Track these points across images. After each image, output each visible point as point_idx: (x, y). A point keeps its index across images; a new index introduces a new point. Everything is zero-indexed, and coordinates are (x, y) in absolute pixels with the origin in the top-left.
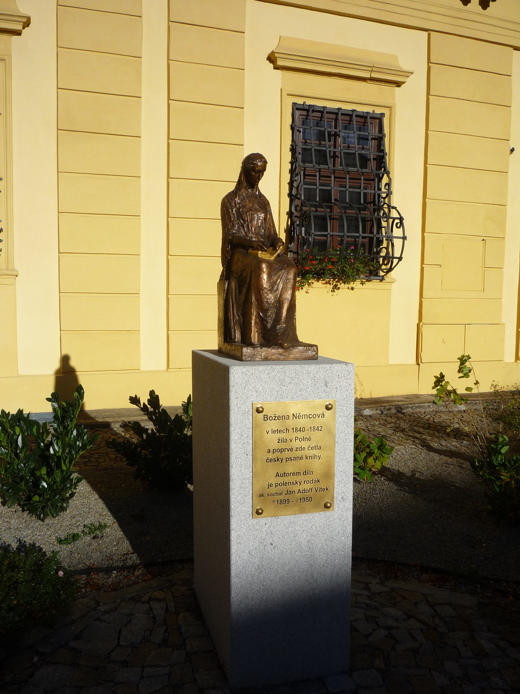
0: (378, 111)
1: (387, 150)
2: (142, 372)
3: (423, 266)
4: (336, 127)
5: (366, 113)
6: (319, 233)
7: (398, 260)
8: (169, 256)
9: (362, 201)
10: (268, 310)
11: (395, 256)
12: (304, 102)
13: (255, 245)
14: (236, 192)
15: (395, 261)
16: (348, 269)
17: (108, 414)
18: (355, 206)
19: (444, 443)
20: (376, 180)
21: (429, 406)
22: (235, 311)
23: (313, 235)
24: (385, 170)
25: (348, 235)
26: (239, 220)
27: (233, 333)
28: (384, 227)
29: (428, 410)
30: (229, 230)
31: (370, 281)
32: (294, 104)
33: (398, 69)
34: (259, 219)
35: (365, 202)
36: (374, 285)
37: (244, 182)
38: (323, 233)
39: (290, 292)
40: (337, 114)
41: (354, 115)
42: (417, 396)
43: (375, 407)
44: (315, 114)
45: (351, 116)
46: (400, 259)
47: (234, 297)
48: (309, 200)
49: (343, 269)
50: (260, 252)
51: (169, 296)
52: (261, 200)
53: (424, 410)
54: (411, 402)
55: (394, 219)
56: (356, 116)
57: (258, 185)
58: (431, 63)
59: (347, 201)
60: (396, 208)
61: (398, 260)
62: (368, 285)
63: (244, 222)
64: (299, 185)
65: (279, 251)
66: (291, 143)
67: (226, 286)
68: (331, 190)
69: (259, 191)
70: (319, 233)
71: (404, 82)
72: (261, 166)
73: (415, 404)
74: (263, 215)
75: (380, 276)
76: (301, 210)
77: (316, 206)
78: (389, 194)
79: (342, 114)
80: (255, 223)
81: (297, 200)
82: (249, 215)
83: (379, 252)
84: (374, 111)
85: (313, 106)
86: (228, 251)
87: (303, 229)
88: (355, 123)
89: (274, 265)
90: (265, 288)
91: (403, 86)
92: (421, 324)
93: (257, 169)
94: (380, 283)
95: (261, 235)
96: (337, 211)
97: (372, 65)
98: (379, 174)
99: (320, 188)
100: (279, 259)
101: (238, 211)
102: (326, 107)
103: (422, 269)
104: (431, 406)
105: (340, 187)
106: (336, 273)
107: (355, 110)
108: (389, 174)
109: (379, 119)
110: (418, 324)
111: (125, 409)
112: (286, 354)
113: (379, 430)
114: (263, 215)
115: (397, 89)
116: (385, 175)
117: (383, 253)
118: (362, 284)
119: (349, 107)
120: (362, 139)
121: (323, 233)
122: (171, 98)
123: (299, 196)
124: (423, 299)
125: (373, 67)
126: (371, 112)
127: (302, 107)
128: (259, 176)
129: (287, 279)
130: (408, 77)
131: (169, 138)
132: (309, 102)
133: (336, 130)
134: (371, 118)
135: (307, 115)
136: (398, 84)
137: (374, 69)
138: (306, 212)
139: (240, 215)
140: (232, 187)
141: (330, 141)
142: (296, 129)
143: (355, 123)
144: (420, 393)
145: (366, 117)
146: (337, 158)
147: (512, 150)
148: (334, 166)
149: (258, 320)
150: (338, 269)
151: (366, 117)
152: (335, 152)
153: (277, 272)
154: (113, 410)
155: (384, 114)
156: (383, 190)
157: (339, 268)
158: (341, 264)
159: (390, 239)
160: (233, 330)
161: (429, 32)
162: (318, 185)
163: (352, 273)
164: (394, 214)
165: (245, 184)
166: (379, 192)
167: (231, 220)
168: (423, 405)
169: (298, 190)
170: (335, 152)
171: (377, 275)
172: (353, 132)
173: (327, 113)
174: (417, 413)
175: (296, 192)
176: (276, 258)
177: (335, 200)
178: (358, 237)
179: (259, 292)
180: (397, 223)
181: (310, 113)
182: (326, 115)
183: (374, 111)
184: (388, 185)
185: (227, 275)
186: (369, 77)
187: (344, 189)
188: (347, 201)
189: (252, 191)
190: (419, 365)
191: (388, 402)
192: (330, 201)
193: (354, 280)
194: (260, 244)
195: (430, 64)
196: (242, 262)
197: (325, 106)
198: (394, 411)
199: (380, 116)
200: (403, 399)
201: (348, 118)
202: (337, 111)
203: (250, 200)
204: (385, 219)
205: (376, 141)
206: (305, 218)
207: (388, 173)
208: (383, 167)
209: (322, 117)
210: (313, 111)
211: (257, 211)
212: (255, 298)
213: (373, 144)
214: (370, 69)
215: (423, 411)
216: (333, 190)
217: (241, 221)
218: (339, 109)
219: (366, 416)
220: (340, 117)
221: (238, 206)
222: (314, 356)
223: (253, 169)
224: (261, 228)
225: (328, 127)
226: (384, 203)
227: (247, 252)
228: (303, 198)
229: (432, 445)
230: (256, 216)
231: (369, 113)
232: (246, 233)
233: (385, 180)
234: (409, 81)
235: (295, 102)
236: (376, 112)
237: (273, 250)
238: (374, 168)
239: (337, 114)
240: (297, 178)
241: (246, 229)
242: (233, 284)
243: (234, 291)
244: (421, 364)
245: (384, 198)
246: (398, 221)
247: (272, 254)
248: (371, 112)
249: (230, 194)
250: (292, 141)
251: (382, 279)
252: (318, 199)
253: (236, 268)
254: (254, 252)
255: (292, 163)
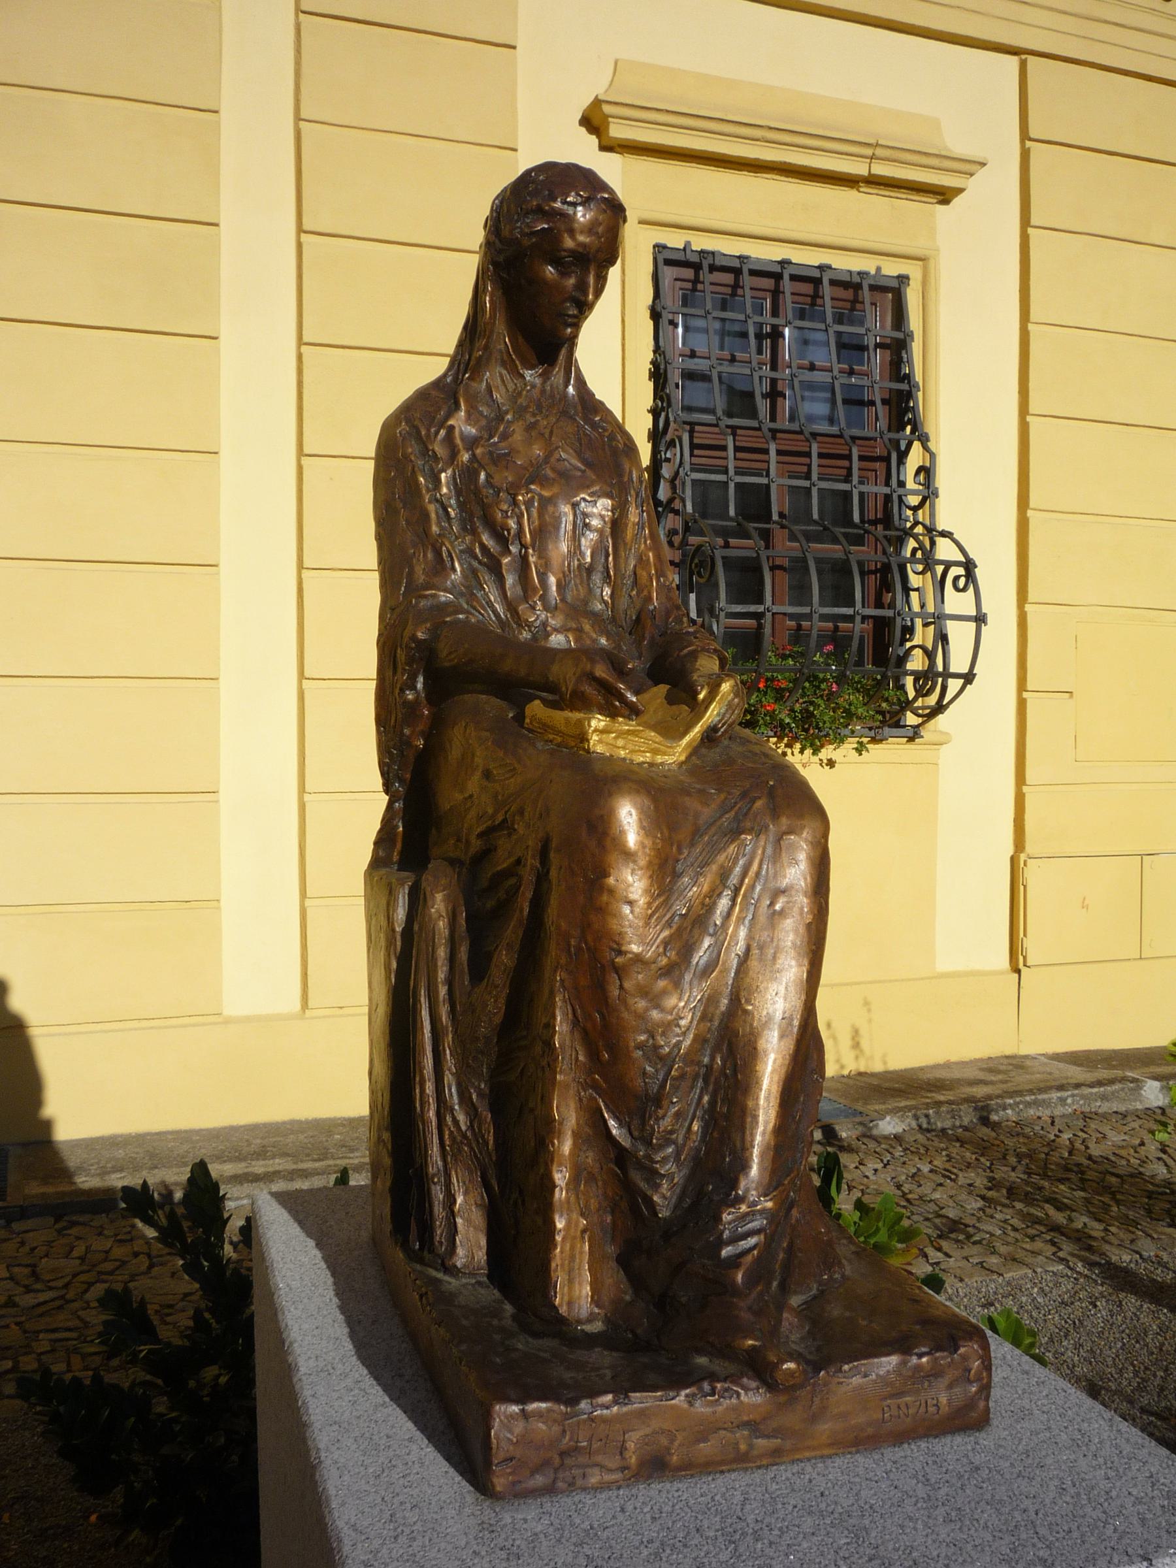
0: (892, 269)
1: (918, 377)
2: (228, 1021)
3: (1025, 695)
4: (775, 313)
5: (859, 273)
6: (739, 608)
7: (961, 681)
8: (304, 681)
9: (856, 517)
10: (658, 1100)
11: (953, 669)
12: (688, 244)
13: (566, 675)
14: (457, 381)
15: (954, 685)
16: (823, 712)
17: (120, 1153)
18: (839, 531)
19: (1149, 1249)
20: (894, 456)
21: (1062, 1100)
22: (449, 1078)
23: (722, 614)
24: (913, 432)
25: (819, 611)
26: (474, 532)
27: (439, 1211)
28: (917, 590)
29: (1059, 1111)
30: (414, 590)
31: (881, 741)
32: (659, 248)
33: (943, 153)
34: (581, 525)
35: (862, 521)
36: (891, 752)
37: (501, 327)
38: (753, 608)
39: (791, 970)
40: (777, 277)
41: (826, 282)
42: (1017, 1063)
43: (909, 1108)
44: (718, 277)
45: (817, 282)
46: (969, 678)
47: (443, 991)
48: (704, 515)
49: (807, 710)
50: (598, 722)
51: (307, 797)
52: (594, 426)
53: (1048, 1112)
54: (1008, 1087)
55: (948, 565)
56: (833, 283)
57: (572, 341)
58: (1031, 139)
59: (816, 516)
60: (952, 534)
61: (961, 681)
62: (876, 751)
63: (502, 540)
64: (677, 473)
65: (712, 714)
66: (651, 356)
67: (401, 914)
68: (768, 487)
69: (581, 383)
70: (739, 608)
71: (961, 190)
72: (591, 229)
73: (1019, 1093)
74: (603, 506)
75: (906, 726)
76: (684, 543)
77: (725, 533)
78: (929, 494)
79: (794, 278)
80: (564, 547)
81: (671, 515)
82: (529, 504)
83: (902, 660)
84: (879, 269)
85: (713, 253)
86: (412, 707)
87: (693, 596)
88: (828, 303)
89: (692, 803)
90: (638, 959)
91: (957, 201)
92: (1023, 857)
93: (569, 243)
94: (908, 746)
95: (595, 616)
96: (785, 547)
97: (872, 141)
98: (898, 442)
99: (739, 479)
100: (714, 754)
101: (468, 475)
102: (747, 257)
103: (1022, 705)
104: (1069, 1101)
105: (790, 477)
106: (787, 720)
107: (829, 267)
108: (928, 440)
109: (893, 293)
110: (1012, 858)
111: (177, 1133)
112: (792, 1419)
113: (937, 1195)
114: (603, 506)
115: (940, 208)
116: (916, 445)
117: (916, 662)
118: (859, 751)
119: (809, 258)
120: (851, 348)
121: (753, 608)
122: (306, 227)
123: (677, 505)
124: (1025, 789)
125: (877, 145)
126: (873, 272)
127: (680, 257)
128: (582, 287)
129: (778, 893)
130: (972, 175)
131: (300, 342)
132: (701, 243)
133: (775, 321)
134: (873, 288)
135: (696, 281)
136: (944, 195)
137: (879, 152)
138: (699, 547)
139: (477, 508)
140: (437, 368)
141: (760, 352)
142: (666, 316)
143: (828, 303)
144: (1024, 1051)
145: (857, 287)
146: (780, 400)
147: (1084, 906)
148: (773, 418)
149: (590, 1158)
150: (792, 710)
151: (857, 287)
152: (774, 382)
153: (714, 850)
154: (139, 1139)
155: (907, 278)
156: (910, 484)
157: (797, 707)
158: (803, 696)
159: (938, 620)
160: (438, 1194)
161: (1023, 57)
162: (731, 472)
163: (833, 721)
164: (945, 550)
165: (503, 339)
166: (901, 491)
167: (426, 532)
168: (1045, 1096)
169: (674, 488)
170: (774, 382)
171: (897, 725)
172: (823, 326)
173: (753, 273)
174: (1031, 1125)
175: (669, 494)
176: (695, 751)
177: (781, 515)
178: (808, 617)
179: (599, 987)
180: (957, 578)
181: (705, 275)
182: (747, 281)
183: (879, 269)
184: (926, 472)
185: (410, 842)
186: (866, 173)
187: (806, 484)
188: (816, 516)
189: (545, 376)
190: (1019, 972)
191: (938, 1085)
192: (768, 518)
193: (840, 740)
194: (601, 671)
195: (1028, 144)
196: (487, 775)
197: (745, 253)
198: (968, 1117)
199: (895, 284)
200: (982, 1076)
201: (807, 288)
202: (778, 269)
203: (530, 427)
204: (920, 568)
205: (888, 352)
206: (701, 564)
207: (924, 440)
208: (909, 422)
209: (736, 286)
210: (713, 268)
211: (570, 483)
212: (575, 1022)
213: (878, 359)
214: (869, 152)
215: (1045, 1113)
216: (773, 487)
217: (486, 538)
218: (784, 263)
219: (886, 1138)
220: (787, 285)
221: (465, 457)
222: (970, 1404)
223: (548, 247)
224: (597, 578)
225: (754, 312)
226: (916, 523)
227: (520, 718)
228: (689, 508)
229: (1114, 1259)
230: (566, 509)
231: (867, 273)
232: (511, 607)
233: (915, 458)
234: (975, 187)
235: (662, 241)
236: (885, 272)
237: (671, 700)
238: (883, 424)
239: (777, 277)
240: (673, 454)
241: (510, 580)
242: (438, 905)
243: (442, 953)
244: (1024, 970)
245: (915, 509)
246: (961, 571)
247: (672, 731)
248: (873, 272)
249: (422, 395)
250: (655, 352)
251: (914, 735)
252: (732, 512)
253: (467, 794)
254: (560, 717)
255: (655, 412)
